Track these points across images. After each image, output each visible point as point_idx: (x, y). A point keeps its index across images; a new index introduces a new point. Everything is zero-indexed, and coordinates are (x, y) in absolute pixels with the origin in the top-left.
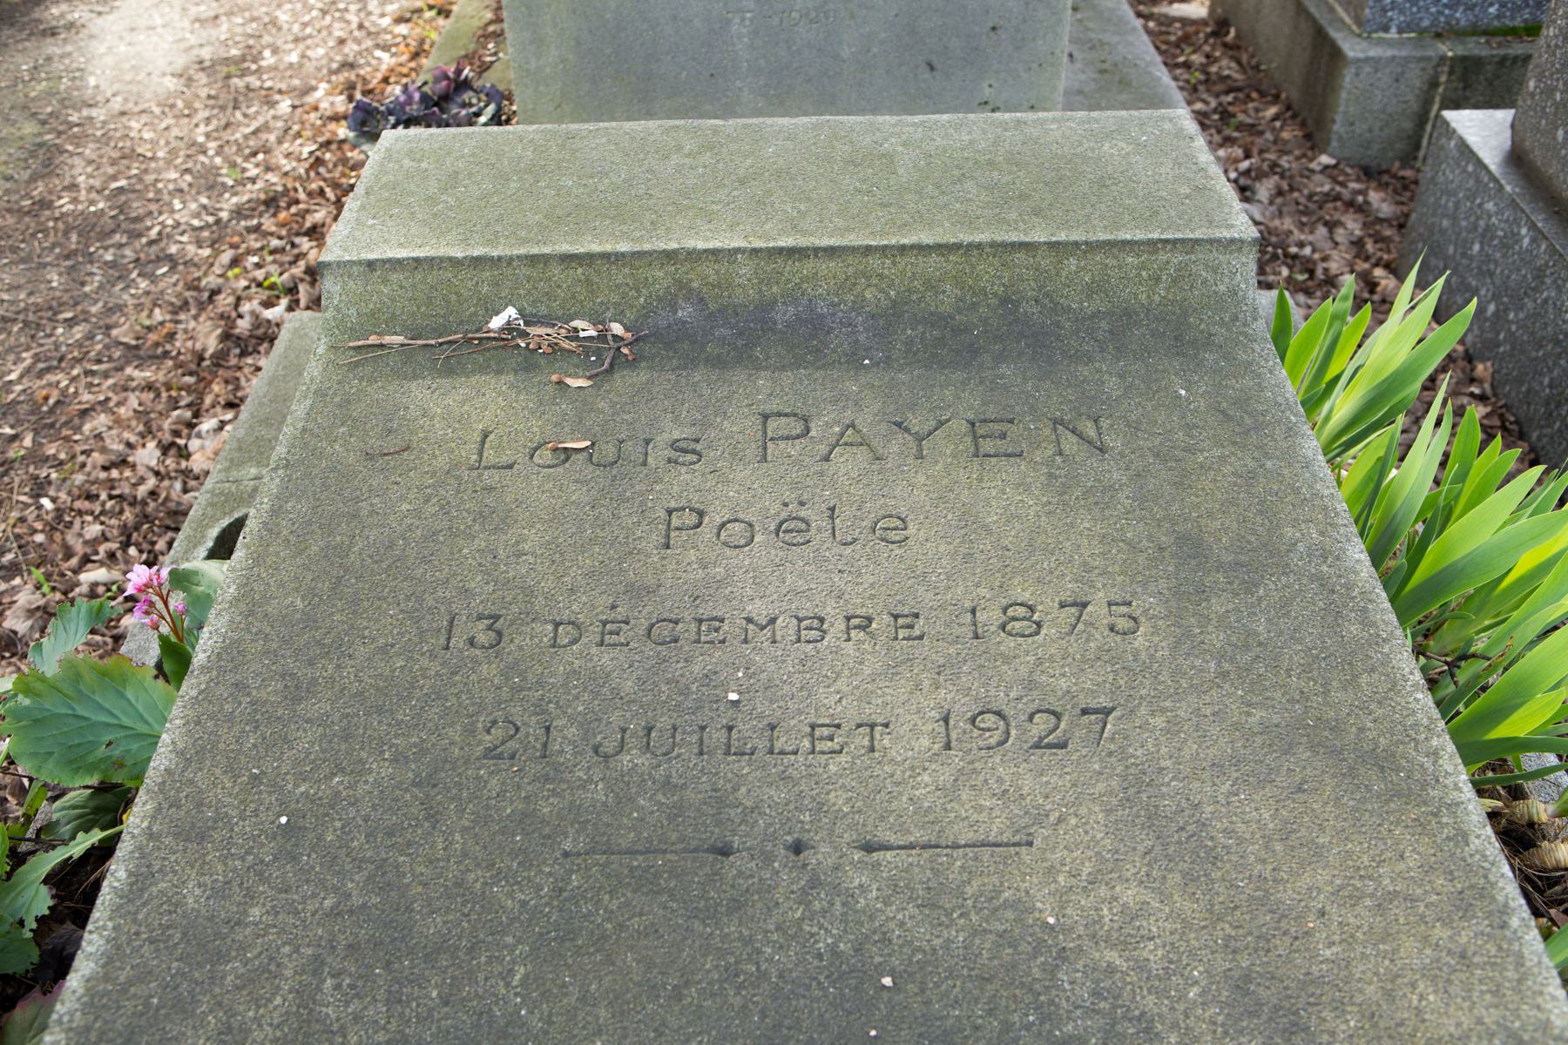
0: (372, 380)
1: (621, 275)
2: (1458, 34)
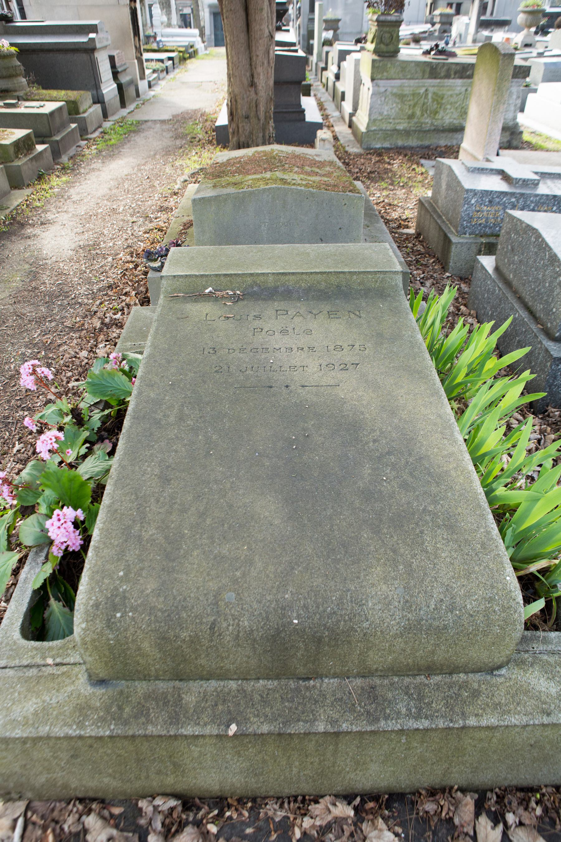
0: (176, 303)
1: (239, 280)
2: (488, 236)
